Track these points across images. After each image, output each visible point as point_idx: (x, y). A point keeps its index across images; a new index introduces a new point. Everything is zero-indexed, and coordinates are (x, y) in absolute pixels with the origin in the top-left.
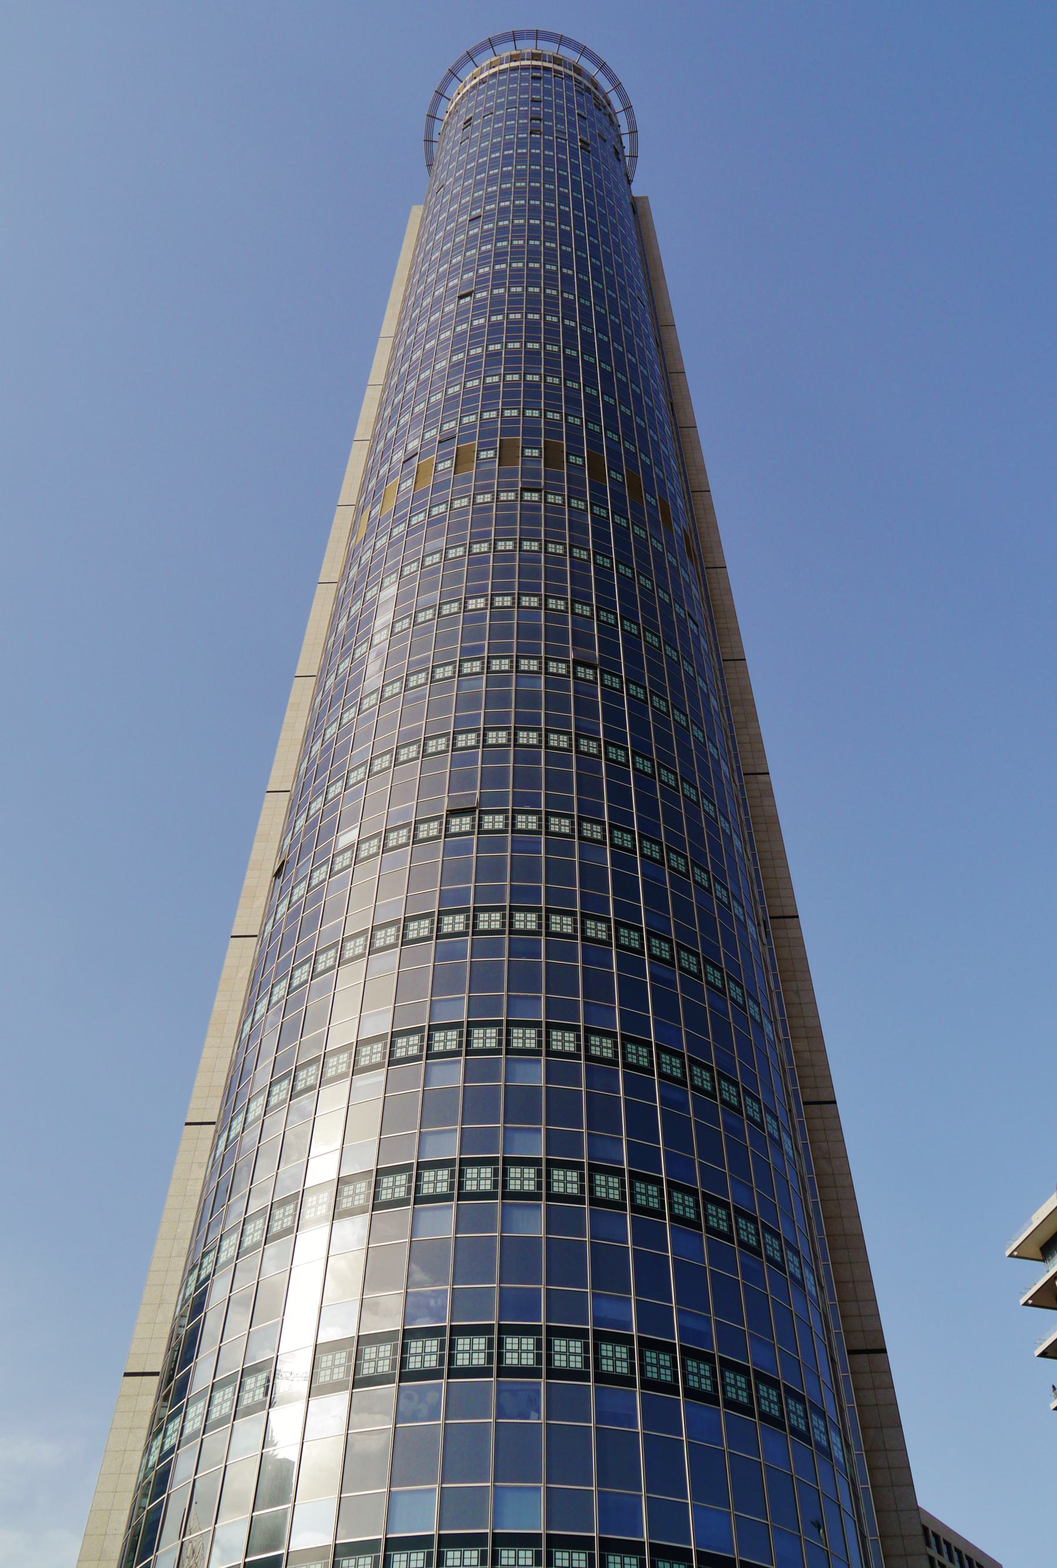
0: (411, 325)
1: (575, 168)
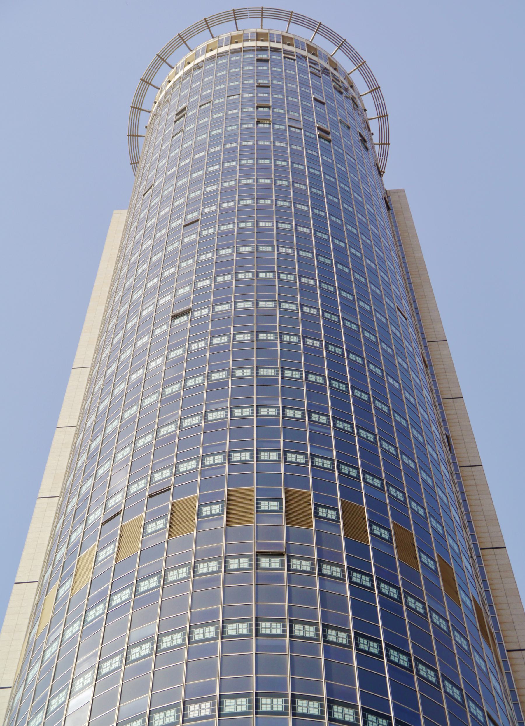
0: (106, 384)
1: (313, 160)
